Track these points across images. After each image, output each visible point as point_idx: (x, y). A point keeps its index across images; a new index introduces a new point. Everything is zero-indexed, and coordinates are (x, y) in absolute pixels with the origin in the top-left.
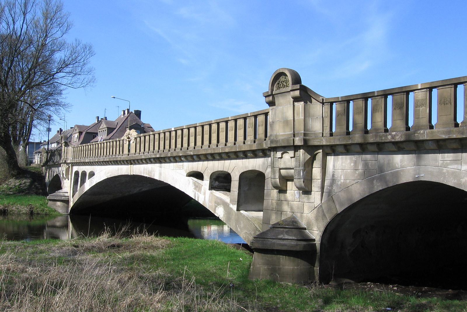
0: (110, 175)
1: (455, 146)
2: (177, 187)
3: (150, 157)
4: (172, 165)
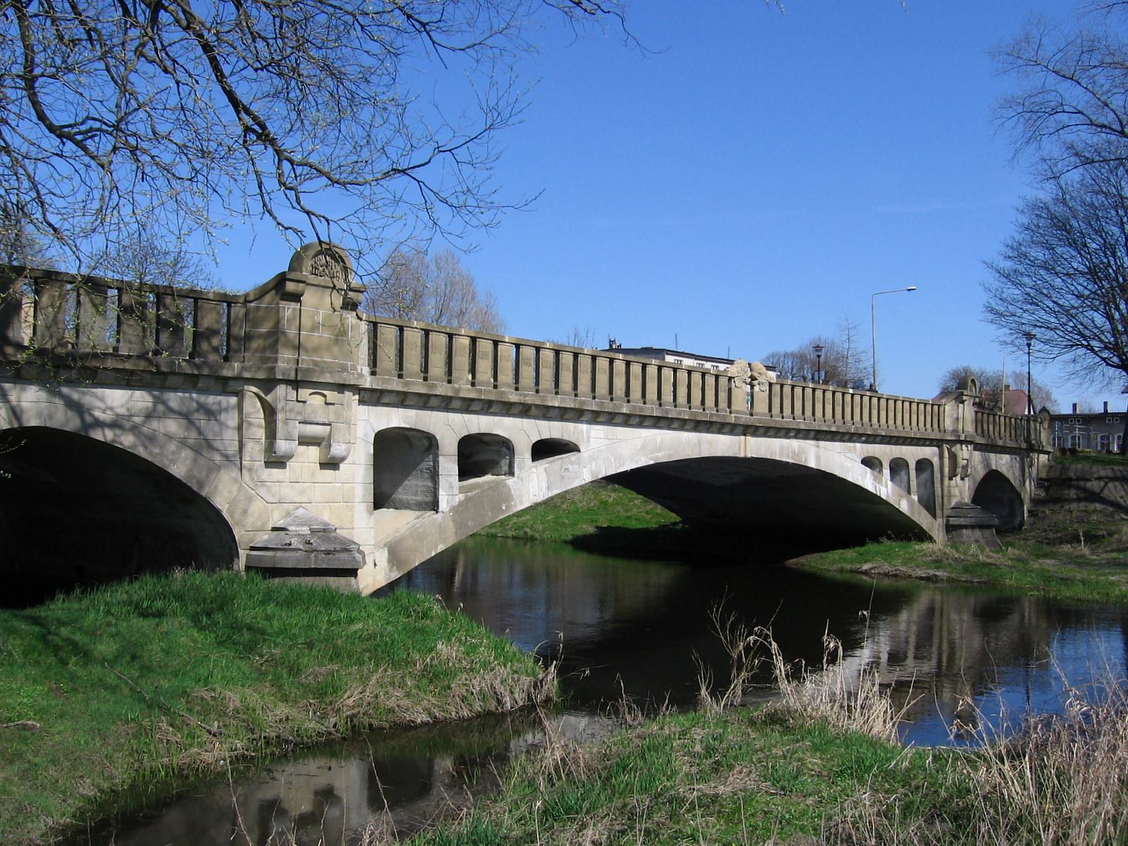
0: (670, 456)
1: (1008, 450)
2: (850, 479)
3: (817, 428)
4: (837, 445)
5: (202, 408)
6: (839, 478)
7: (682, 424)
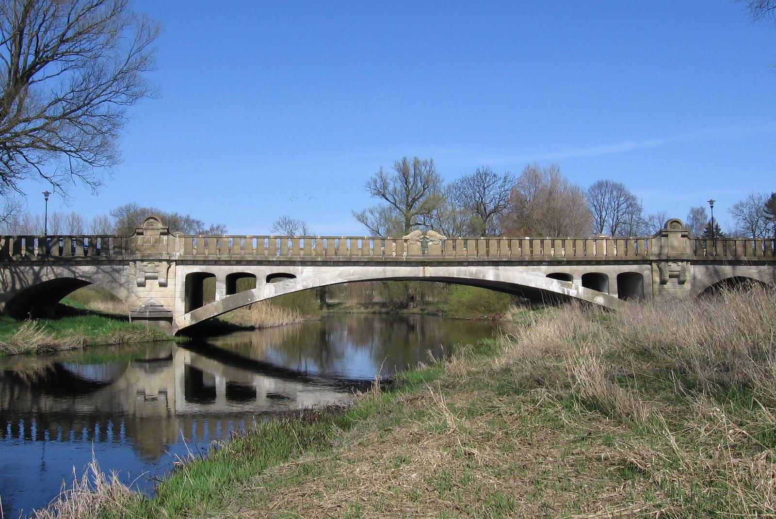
0: (359, 278)
5: (114, 270)
6: (521, 285)
7: (408, 263)
